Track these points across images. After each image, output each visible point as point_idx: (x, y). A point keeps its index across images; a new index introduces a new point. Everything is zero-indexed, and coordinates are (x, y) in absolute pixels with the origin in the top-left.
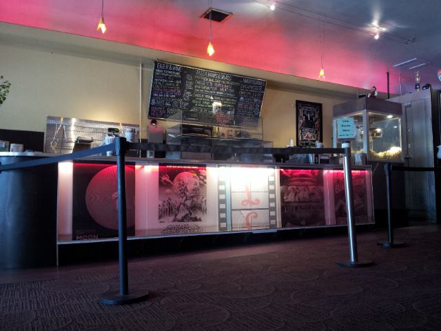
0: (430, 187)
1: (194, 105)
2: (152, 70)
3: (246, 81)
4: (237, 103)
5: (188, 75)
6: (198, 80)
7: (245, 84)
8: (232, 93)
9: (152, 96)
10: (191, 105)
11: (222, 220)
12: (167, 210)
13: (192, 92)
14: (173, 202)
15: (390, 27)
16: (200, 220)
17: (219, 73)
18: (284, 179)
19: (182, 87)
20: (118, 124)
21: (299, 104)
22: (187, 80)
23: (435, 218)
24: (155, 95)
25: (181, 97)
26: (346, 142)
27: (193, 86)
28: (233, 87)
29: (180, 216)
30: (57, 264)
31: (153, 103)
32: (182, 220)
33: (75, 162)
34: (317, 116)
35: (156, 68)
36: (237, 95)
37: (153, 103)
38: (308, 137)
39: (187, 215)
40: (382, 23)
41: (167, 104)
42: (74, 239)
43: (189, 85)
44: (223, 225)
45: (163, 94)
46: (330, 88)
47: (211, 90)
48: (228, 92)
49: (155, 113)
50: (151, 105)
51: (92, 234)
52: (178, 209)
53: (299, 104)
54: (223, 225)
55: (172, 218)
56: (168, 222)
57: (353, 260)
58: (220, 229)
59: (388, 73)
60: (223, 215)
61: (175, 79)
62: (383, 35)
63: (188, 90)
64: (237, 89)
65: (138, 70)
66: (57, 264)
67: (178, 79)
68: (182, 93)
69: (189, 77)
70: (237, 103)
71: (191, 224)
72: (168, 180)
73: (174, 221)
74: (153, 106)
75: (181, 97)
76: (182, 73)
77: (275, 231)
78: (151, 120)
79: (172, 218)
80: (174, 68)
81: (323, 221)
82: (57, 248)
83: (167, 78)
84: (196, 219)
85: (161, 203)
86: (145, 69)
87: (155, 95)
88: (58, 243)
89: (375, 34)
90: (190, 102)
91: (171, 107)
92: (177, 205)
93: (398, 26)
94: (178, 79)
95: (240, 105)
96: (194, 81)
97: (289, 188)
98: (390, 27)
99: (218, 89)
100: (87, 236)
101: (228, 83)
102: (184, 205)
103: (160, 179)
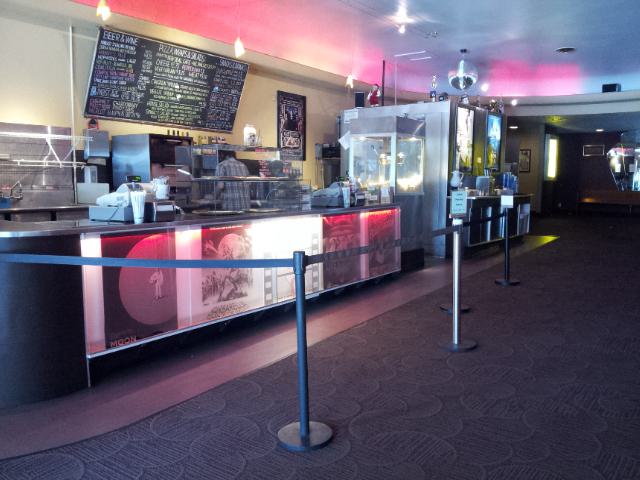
0: (440, 217)
1: (152, 96)
2: (97, 40)
3: (223, 64)
4: (209, 95)
5: (147, 52)
6: (161, 58)
7: (223, 67)
8: (204, 80)
9: (92, 82)
10: (148, 96)
11: (268, 291)
12: (210, 289)
13: (151, 76)
14: (218, 276)
15: (418, 19)
16: (246, 295)
17: (192, 49)
18: (327, 230)
19: (137, 69)
20: (41, 129)
21: (283, 97)
22: (145, 58)
23: (444, 254)
24: (98, 81)
25: (134, 84)
26: (460, 218)
27: (152, 68)
28: (207, 72)
29: (224, 295)
30: (89, 385)
31: (94, 92)
32: (227, 299)
33: (102, 236)
34: (300, 114)
35: (101, 38)
36: (211, 84)
37: (94, 92)
38: (290, 143)
39: (232, 291)
40: (411, 12)
41: (114, 95)
42: (108, 347)
43: (147, 66)
44: (269, 297)
45: (109, 79)
46: (311, 75)
47: (176, 75)
48: (199, 78)
49: (97, 107)
50: (90, 97)
51: (129, 335)
52: (223, 284)
53: (283, 97)
54: (269, 297)
55: (217, 297)
56: (213, 302)
57: (456, 342)
58: (266, 301)
59: (384, 63)
60: (269, 285)
61: (128, 56)
62: (409, 27)
63: (145, 74)
64: (211, 74)
65: (66, 37)
66: (89, 385)
67: (132, 57)
68: (137, 78)
69: (148, 54)
70: (209, 95)
71: (238, 301)
72: (213, 248)
73: (219, 300)
74: (94, 97)
75: (134, 84)
76: (138, 49)
77: (317, 295)
78: (89, 120)
79: (217, 297)
80: (127, 40)
81: (357, 274)
82: (88, 362)
83: (115, 54)
84: (241, 295)
85: (204, 279)
86: (77, 36)
87: (98, 81)
88: (89, 357)
89: (400, 25)
90: (146, 92)
91: (119, 100)
92: (222, 280)
93: (428, 20)
94: (132, 57)
95: (213, 99)
96: (154, 59)
97: (331, 239)
98: (418, 19)
99: (187, 74)
100: (125, 338)
101: (200, 65)
102: (230, 278)
103: (203, 247)
